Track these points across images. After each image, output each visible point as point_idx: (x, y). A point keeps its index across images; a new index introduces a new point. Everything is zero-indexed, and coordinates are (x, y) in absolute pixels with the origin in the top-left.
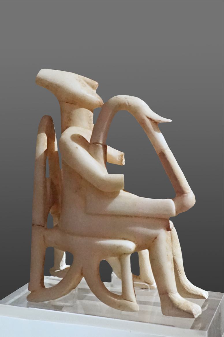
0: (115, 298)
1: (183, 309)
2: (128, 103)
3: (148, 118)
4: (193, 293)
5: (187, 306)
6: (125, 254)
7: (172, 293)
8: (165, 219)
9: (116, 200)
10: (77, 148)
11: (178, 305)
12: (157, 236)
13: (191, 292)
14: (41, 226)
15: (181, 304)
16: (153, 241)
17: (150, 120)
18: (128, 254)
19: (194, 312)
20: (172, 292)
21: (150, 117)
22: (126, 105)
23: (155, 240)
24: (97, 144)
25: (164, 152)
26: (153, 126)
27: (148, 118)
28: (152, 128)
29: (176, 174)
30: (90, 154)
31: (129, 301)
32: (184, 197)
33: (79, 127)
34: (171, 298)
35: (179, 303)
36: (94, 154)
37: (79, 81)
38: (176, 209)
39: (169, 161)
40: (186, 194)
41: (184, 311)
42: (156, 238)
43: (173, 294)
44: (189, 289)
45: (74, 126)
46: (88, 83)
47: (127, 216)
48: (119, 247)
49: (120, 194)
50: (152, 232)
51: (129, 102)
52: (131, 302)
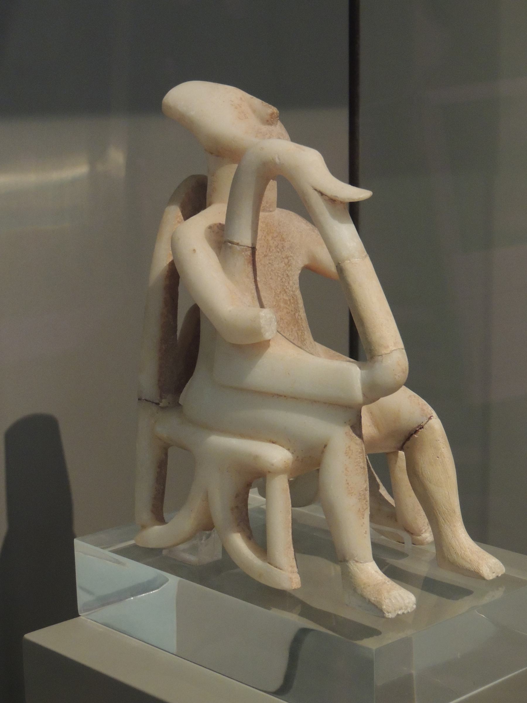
2: (279, 158)
3: (316, 190)
14: (153, 403)
15: (369, 586)
20: (356, 559)
21: (319, 188)
24: (230, 244)
35: (365, 584)
40: (380, 358)
41: (369, 601)
42: (325, 446)
43: (357, 564)
45: (210, 205)
46: (254, 111)
47: (279, 396)
52: (279, 570)
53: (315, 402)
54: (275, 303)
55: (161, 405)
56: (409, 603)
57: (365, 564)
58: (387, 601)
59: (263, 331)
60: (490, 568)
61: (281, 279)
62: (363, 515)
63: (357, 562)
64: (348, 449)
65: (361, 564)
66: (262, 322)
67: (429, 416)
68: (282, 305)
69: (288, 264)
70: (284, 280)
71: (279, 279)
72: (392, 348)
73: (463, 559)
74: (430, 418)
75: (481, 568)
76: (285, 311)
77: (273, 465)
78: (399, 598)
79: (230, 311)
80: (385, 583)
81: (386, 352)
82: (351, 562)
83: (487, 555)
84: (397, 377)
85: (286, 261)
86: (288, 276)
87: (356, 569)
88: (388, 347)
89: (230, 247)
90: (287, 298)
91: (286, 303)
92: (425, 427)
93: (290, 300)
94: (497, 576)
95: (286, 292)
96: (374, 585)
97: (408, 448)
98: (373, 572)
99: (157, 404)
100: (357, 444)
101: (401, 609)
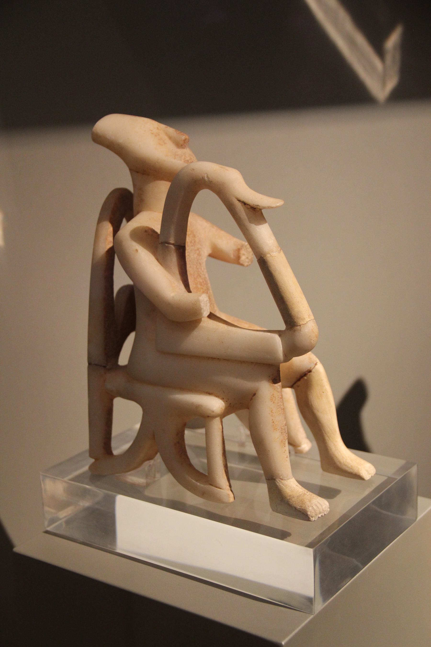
0: (197, 481)
1: (295, 505)
2: (207, 177)
3: (239, 201)
4: (347, 469)
5: (302, 501)
6: (208, 416)
7: (282, 479)
8: (269, 365)
9: (195, 333)
10: (137, 250)
11: (288, 498)
12: (257, 391)
13: (344, 467)
14: (101, 366)
15: (294, 497)
16: (252, 399)
17: (243, 204)
18: (214, 417)
19: (310, 512)
20: (281, 477)
21: (242, 199)
22: (205, 181)
23: (254, 397)
24: (167, 245)
25: (265, 258)
26: (247, 215)
27: (239, 201)
28: (246, 218)
29: (283, 294)
30: (157, 260)
31: (217, 487)
32: (295, 331)
33: (155, 212)
34: (279, 487)
35: (290, 496)
36: (162, 260)
37: (156, 136)
38: (284, 351)
39: (273, 272)
40: (298, 327)
41: (296, 508)
42: (255, 394)
43: (283, 481)
44: (340, 462)
45: (138, 213)
46: (170, 138)
47: (213, 358)
48: (198, 407)
49: (202, 324)
50: (247, 385)
51: (209, 176)
52: (219, 489)
53: (244, 362)
54: (195, 286)
55: (108, 367)
56: (325, 508)
57: (288, 481)
58: (310, 508)
59: (202, 311)
60: (367, 471)
61: (196, 267)
62: (285, 444)
63: (282, 479)
64: (272, 396)
65: (285, 481)
66: (202, 305)
67: (315, 363)
68: (199, 286)
69: (199, 255)
70: (198, 267)
71: (195, 267)
72: (307, 319)
73: (346, 465)
74: (316, 364)
75: (361, 472)
76: (202, 290)
77: (213, 412)
78: (318, 505)
79: (173, 297)
80: (305, 494)
81: (304, 323)
82: (277, 480)
83: (363, 461)
84: (312, 341)
85: (198, 252)
86: (200, 264)
87: (282, 485)
88: (304, 319)
89: (167, 247)
90: (201, 281)
91: (201, 285)
92: (313, 370)
93: (203, 282)
94: (372, 476)
95: (200, 276)
96: (298, 496)
97: (298, 386)
98: (295, 486)
99: (105, 367)
100: (278, 392)
101: (320, 513)
